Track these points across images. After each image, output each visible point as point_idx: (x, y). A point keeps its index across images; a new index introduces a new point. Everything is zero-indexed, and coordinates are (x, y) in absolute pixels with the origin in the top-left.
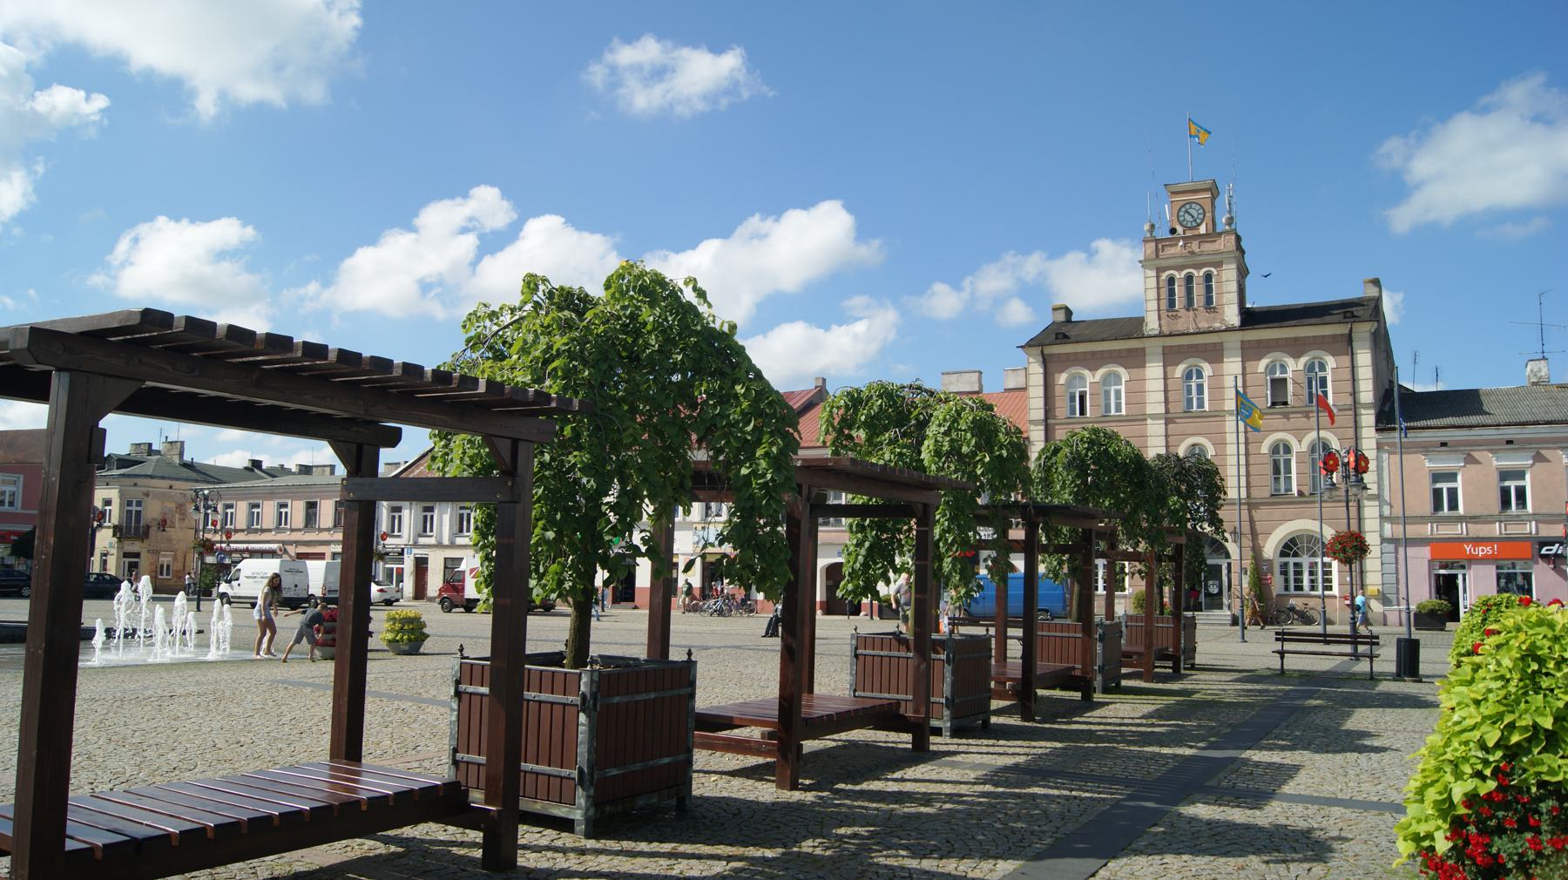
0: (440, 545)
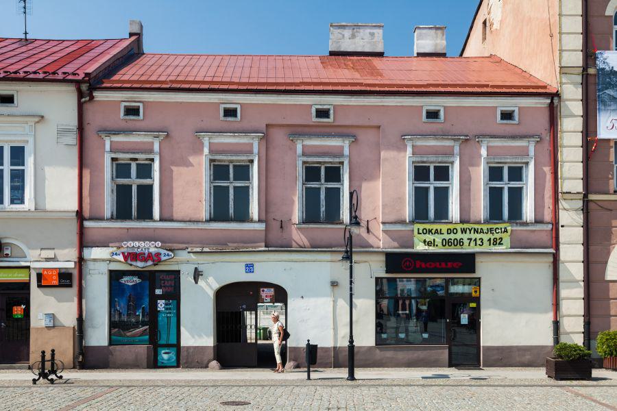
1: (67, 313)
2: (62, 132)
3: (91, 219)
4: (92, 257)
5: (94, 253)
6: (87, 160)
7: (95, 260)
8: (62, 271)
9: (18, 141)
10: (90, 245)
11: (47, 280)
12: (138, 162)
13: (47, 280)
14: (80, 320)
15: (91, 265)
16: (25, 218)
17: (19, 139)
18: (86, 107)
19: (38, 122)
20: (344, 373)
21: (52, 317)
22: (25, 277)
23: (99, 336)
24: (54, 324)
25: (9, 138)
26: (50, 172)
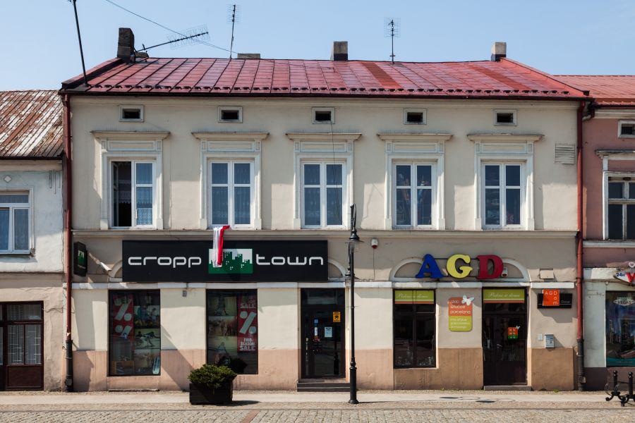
1: (566, 333)
2: (560, 151)
3: (588, 239)
4: (592, 278)
5: (596, 273)
6: (585, 180)
7: (594, 281)
8: (562, 292)
9: (425, 160)
10: (588, 265)
11: (548, 300)
12: (631, 181)
13: (548, 300)
14: (581, 342)
15: (589, 286)
16: (524, 237)
17: (232, 156)
18: (585, 125)
19: (166, 138)
20: (346, 397)
21: (551, 337)
22: (520, 297)
23: (598, 358)
24: (554, 347)
25: (505, 158)
26: (277, 191)
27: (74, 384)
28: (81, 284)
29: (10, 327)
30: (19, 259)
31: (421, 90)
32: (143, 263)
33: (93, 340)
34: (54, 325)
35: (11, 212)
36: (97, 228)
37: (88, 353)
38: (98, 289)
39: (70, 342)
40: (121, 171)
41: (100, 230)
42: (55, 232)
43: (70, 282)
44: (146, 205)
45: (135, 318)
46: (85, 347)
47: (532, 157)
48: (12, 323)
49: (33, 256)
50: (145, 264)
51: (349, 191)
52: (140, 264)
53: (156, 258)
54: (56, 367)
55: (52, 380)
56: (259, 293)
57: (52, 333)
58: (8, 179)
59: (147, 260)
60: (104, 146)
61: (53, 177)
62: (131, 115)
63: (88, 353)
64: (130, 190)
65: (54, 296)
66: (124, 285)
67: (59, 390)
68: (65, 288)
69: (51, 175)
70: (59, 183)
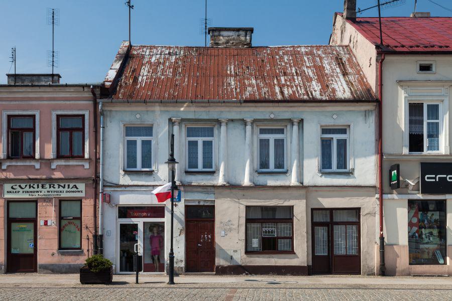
0: (232, 187)
27: (384, 271)
28: (389, 195)
29: (335, 227)
30: (343, 176)
31: (403, 46)
32: (436, 180)
33: (397, 238)
34: (370, 227)
35: (334, 140)
36: (400, 153)
37: (395, 247)
38: (402, 199)
39: (382, 238)
40: (415, 109)
41: (401, 155)
42: (369, 155)
43: (382, 193)
44: (434, 134)
45: (419, 221)
46: (392, 242)
47: (448, 97)
48: (338, 223)
49: (352, 174)
50: (437, 180)
51: (446, 126)
52: (434, 180)
53: (445, 176)
54: (371, 256)
55: (368, 267)
56: (448, 203)
57: (368, 232)
58: (335, 117)
59: (439, 178)
60: (406, 92)
61: (367, 115)
62: (425, 68)
63: (395, 247)
64: (423, 124)
65: (368, 204)
66: (420, 196)
67: (373, 274)
68: (377, 198)
69: (366, 114)
70: (372, 120)
